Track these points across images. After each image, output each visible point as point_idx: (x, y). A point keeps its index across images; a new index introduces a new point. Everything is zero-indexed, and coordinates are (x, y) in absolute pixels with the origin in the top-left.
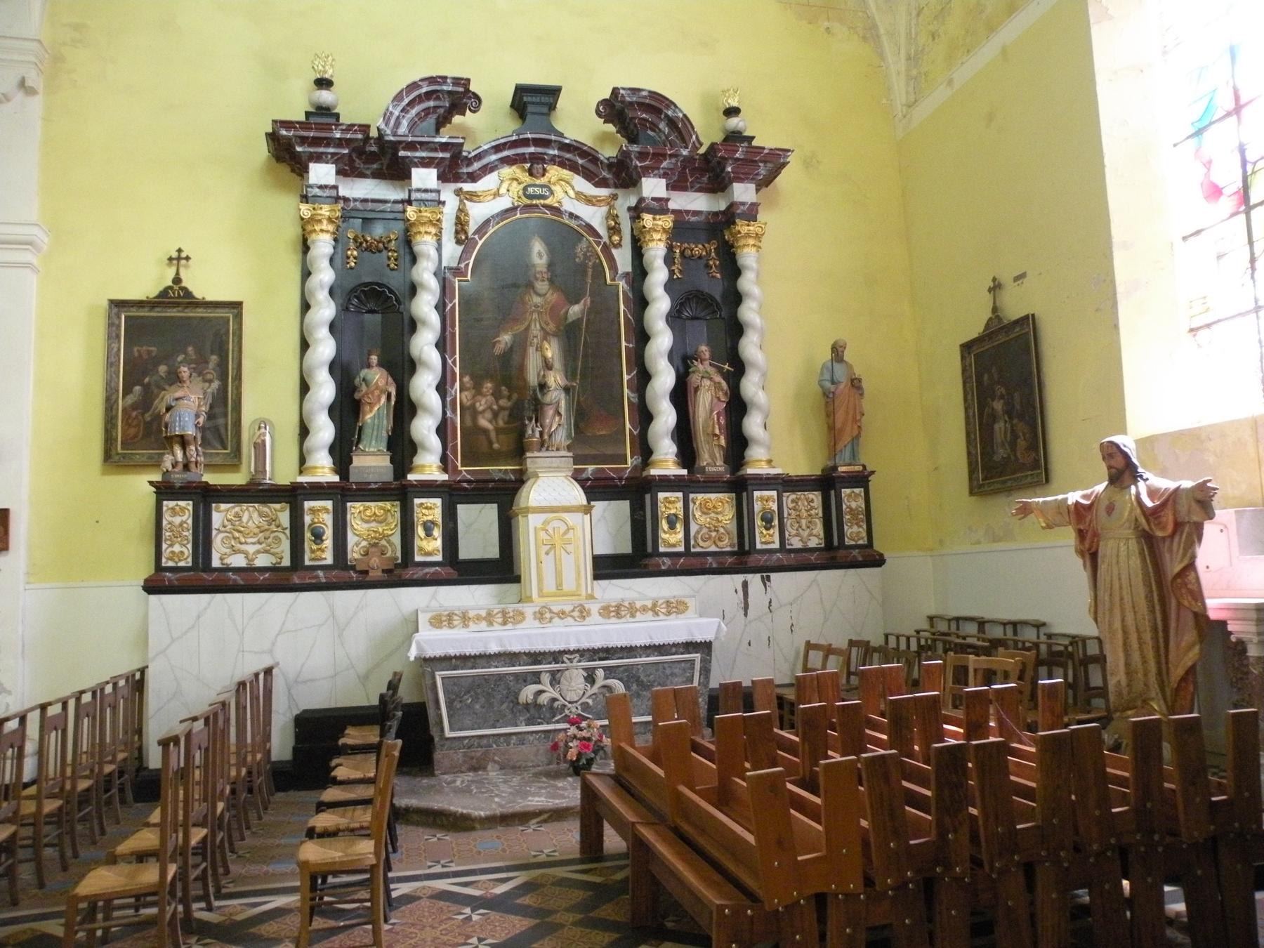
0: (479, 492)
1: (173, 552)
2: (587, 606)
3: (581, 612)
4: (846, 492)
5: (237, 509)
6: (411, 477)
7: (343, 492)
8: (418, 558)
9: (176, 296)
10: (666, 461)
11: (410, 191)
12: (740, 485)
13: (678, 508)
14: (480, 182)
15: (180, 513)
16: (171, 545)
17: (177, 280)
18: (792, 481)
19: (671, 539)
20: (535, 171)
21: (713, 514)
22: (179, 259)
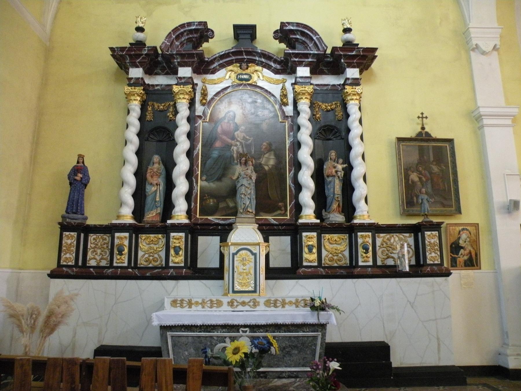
0: (209, 229)
1: (66, 258)
2: (258, 300)
3: (254, 303)
4: (427, 233)
5: (388, 236)
6: (169, 222)
7: (136, 230)
8: (305, 264)
9: (423, 137)
10: (308, 215)
11: (296, 78)
12: (350, 229)
13: (314, 242)
14: (217, 73)
15: (70, 239)
16: (431, 253)
17: (423, 128)
18: (433, 225)
19: (310, 258)
20: (242, 67)
21: (336, 247)
22: (422, 118)
